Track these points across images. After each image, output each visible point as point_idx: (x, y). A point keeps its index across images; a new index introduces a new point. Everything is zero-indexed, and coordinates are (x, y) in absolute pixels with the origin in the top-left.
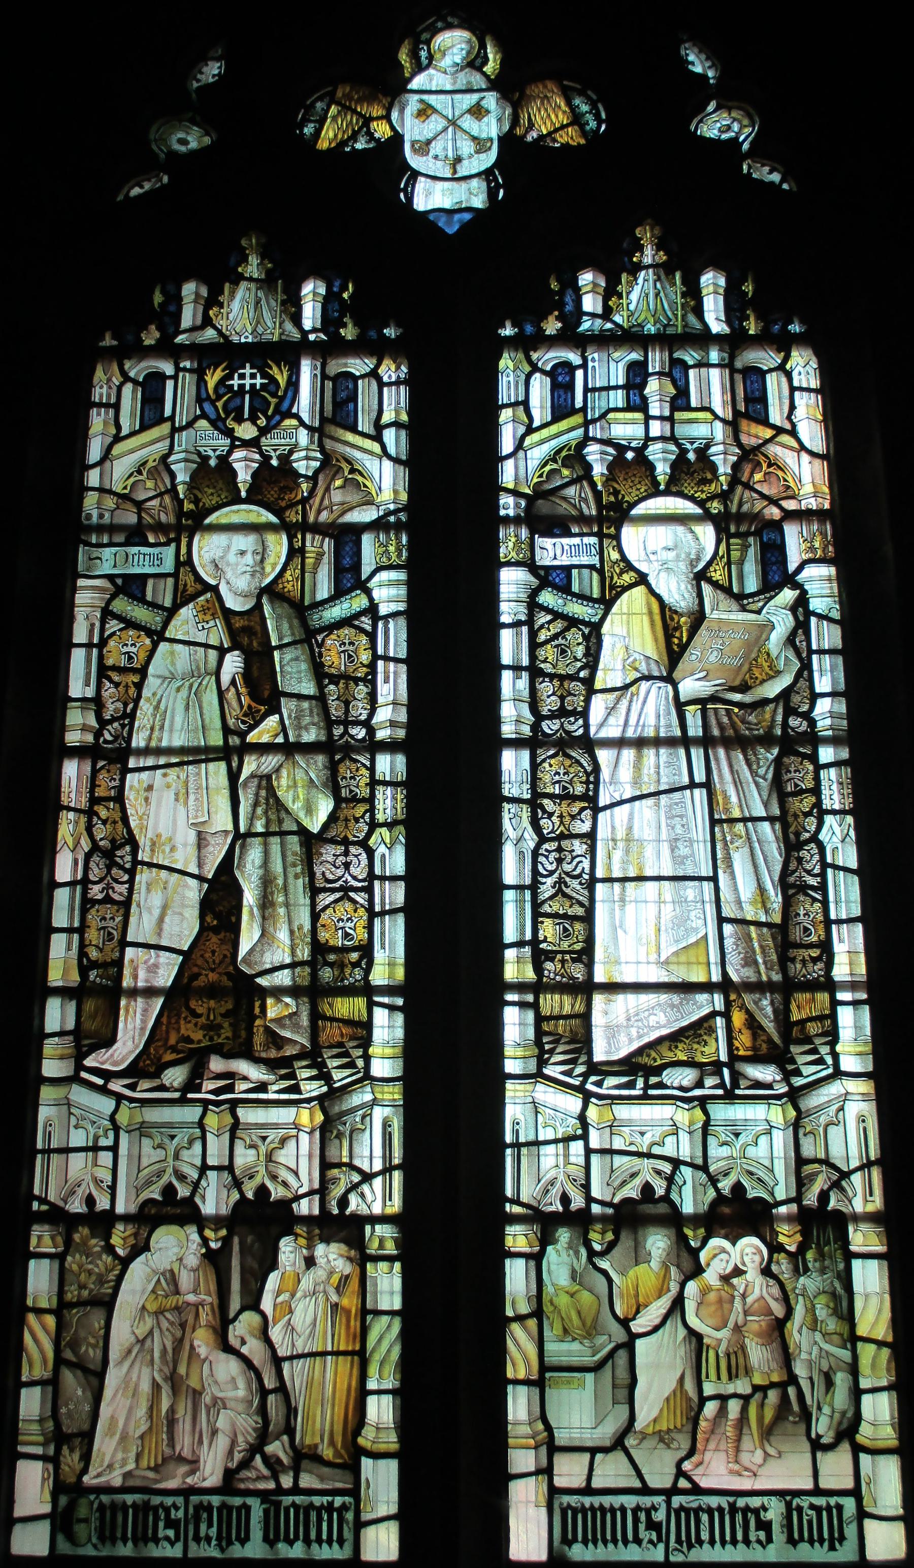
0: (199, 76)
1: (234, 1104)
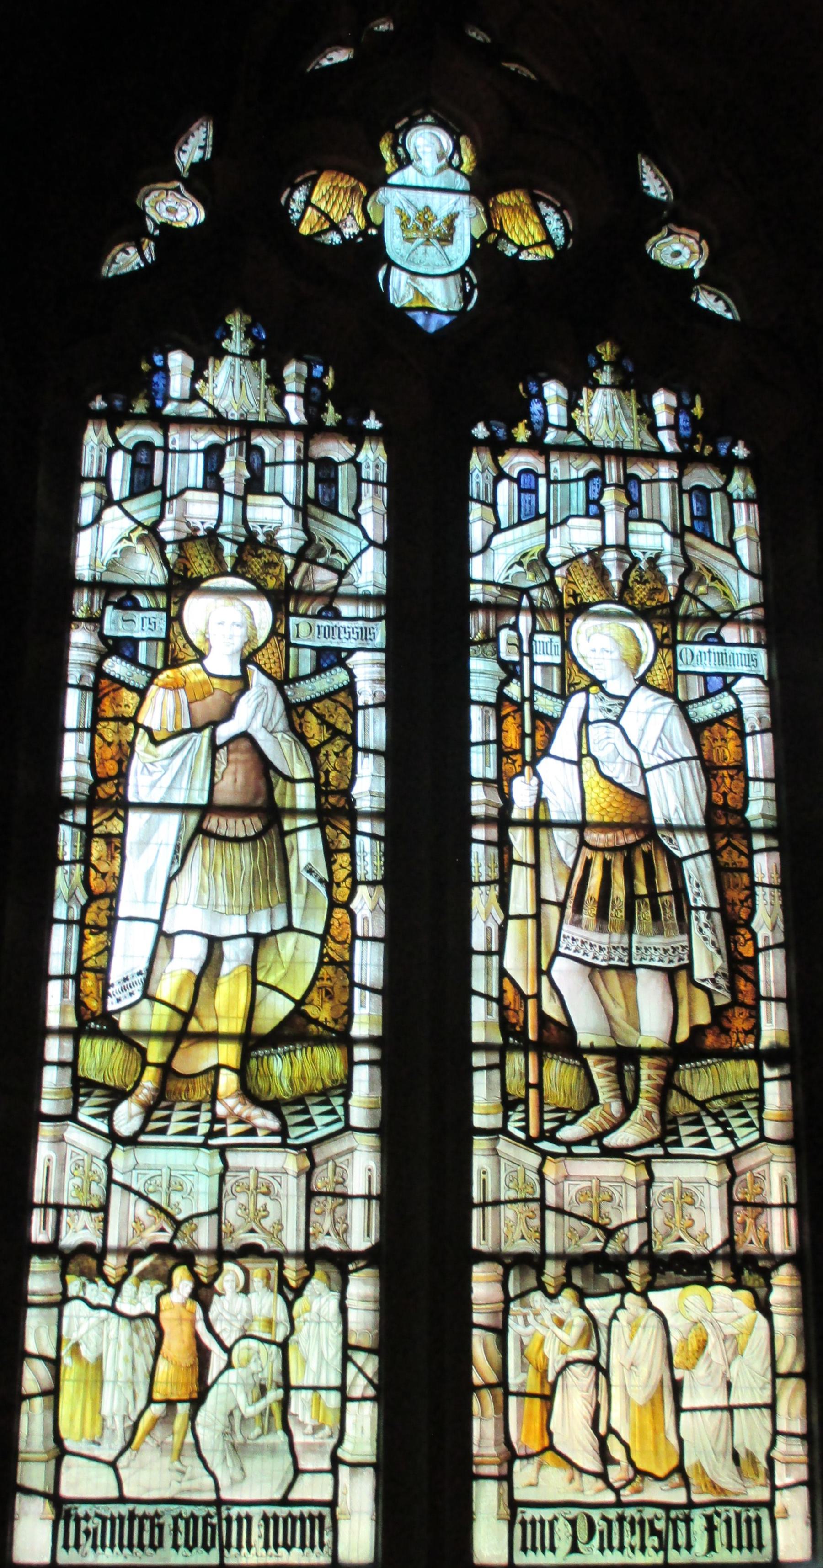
1: (223, 1150)
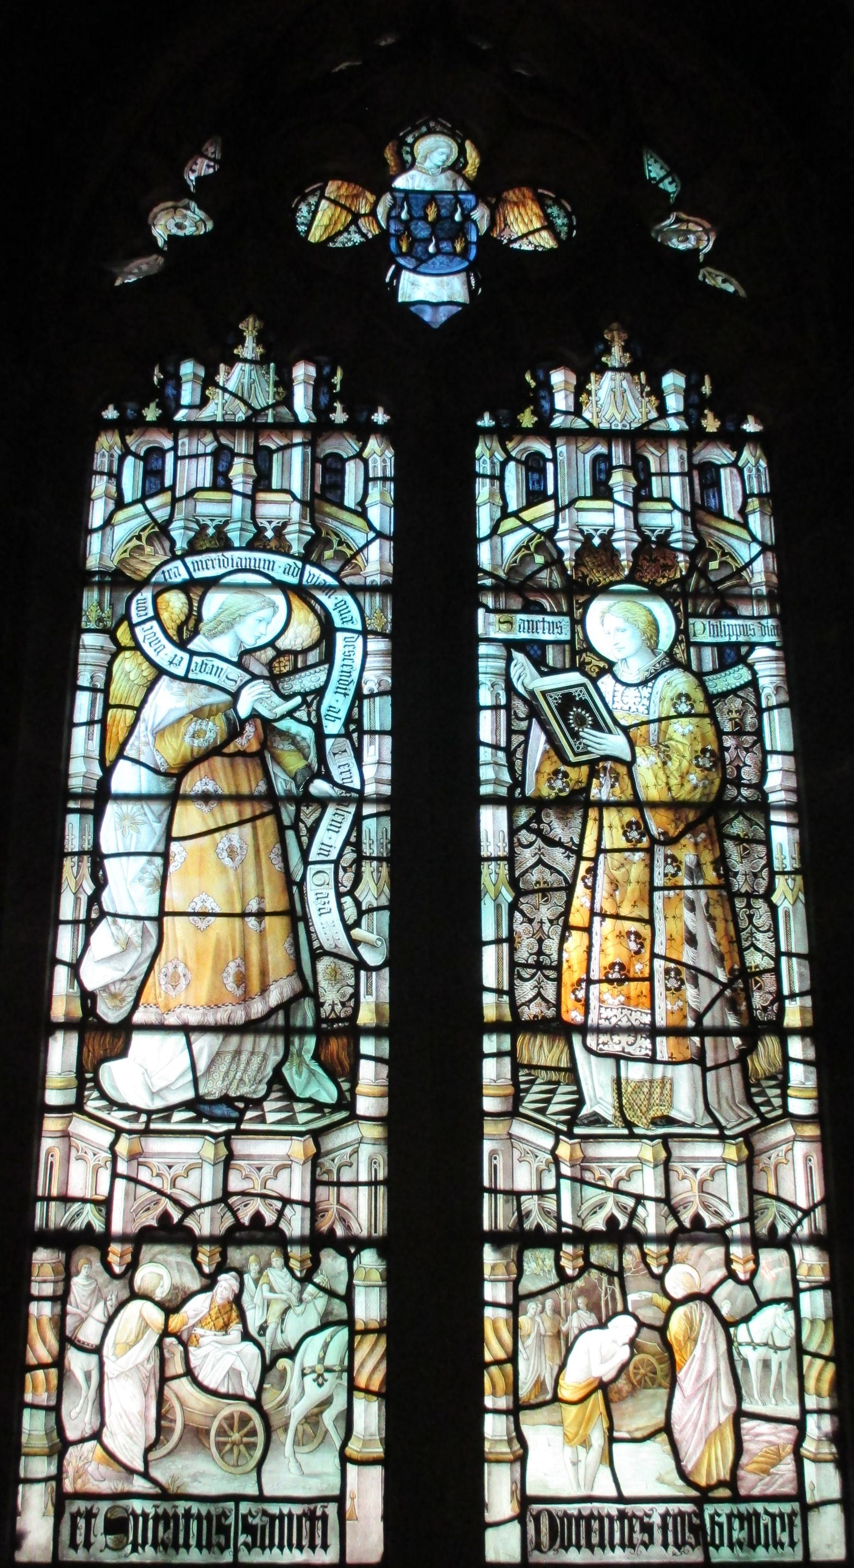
0: (670, 179)
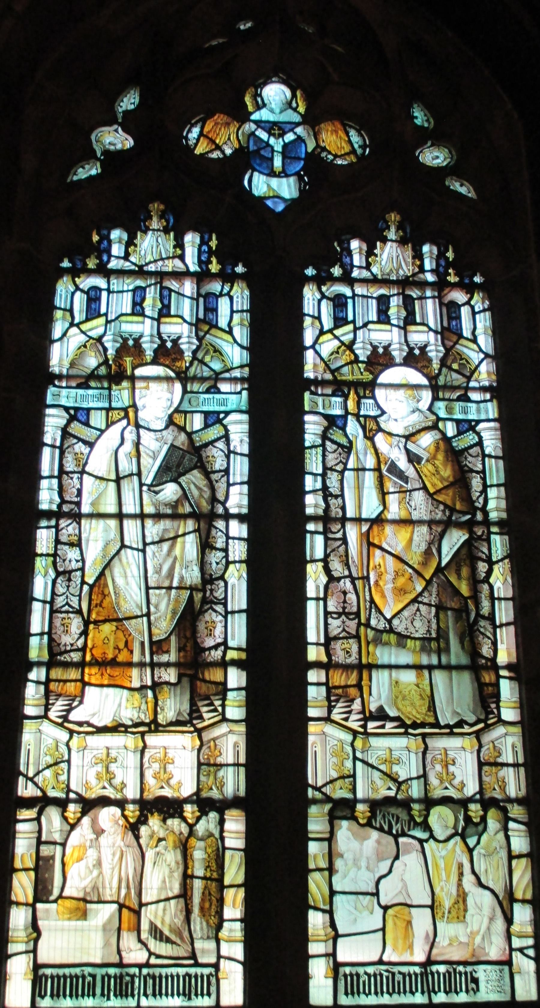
0: (121, 104)
